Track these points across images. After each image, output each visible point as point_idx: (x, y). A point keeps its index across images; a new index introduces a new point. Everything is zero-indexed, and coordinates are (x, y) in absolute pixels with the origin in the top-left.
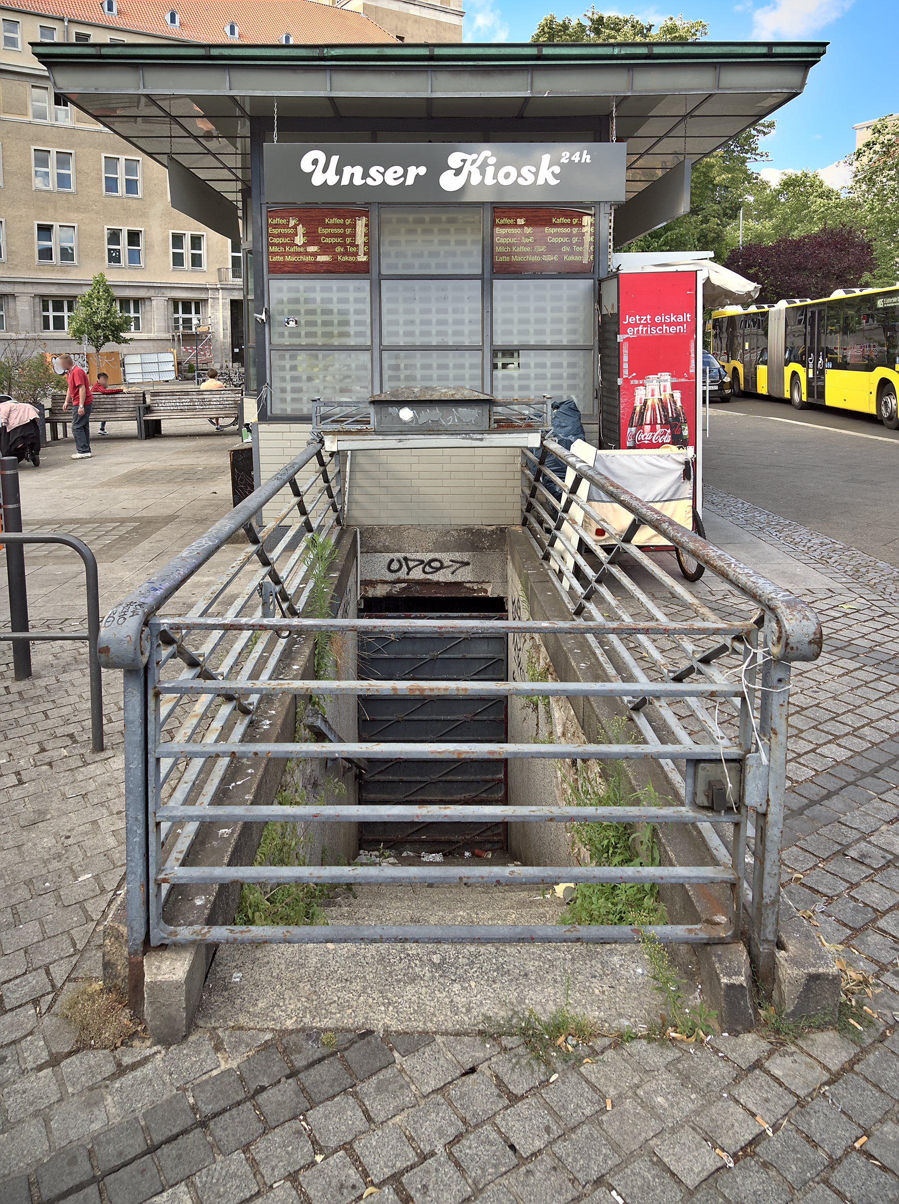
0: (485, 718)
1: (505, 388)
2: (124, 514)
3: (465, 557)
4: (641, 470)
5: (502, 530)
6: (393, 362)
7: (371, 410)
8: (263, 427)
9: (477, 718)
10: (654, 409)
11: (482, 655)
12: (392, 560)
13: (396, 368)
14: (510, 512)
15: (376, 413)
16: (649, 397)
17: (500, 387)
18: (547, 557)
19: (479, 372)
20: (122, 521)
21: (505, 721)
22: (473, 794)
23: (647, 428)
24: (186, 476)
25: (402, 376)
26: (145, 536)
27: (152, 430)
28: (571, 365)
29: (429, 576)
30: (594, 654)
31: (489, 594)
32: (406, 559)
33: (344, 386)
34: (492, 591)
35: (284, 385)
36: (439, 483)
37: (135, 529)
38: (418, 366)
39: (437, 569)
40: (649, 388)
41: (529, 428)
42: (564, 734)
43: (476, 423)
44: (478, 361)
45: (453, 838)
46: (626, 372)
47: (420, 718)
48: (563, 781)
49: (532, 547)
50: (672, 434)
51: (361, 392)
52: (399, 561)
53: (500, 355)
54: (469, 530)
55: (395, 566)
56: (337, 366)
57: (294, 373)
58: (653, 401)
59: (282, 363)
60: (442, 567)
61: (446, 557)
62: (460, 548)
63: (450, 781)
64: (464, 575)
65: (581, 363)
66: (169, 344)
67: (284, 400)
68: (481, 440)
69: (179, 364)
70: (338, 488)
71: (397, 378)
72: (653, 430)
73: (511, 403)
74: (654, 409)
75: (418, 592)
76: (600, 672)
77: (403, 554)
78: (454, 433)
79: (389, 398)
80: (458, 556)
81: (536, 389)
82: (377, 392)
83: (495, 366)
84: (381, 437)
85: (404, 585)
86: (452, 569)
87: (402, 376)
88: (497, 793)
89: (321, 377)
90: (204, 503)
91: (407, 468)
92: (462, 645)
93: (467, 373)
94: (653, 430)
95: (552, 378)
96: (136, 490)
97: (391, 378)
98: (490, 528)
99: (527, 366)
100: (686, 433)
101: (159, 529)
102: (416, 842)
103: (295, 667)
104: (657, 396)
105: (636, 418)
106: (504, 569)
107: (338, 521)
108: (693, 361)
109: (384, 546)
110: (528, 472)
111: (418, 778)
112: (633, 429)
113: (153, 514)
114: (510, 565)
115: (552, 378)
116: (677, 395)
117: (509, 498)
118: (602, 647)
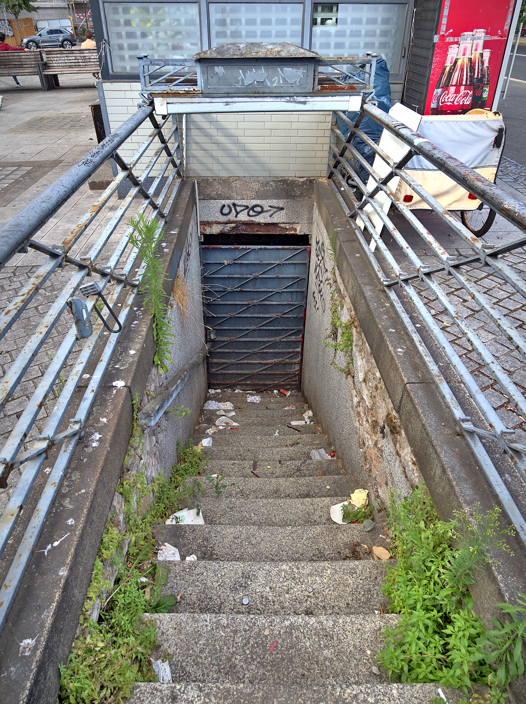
0: (290, 316)
1: (322, 46)
2: (22, 158)
3: (280, 203)
4: (456, 138)
5: (311, 181)
6: (219, 16)
7: (198, 69)
8: (107, 86)
9: (285, 316)
10: (462, 70)
11: (290, 276)
12: (224, 206)
13: (222, 23)
14: (320, 167)
15: (203, 73)
16: (460, 56)
17: (318, 45)
18: (354, 217)
19: (299, 28)
20: (20, 165)
21: (304, 318)
22: (280, 360)
23: (452, 89)
24: (73, 123)
25: (229, 32)
26: (35, 180)
27: (52, 84)
28: (385, 21)
29: (253, 219)
30: (412, 341)
31: (298, 232)
32: (234, 205)
33: (176, 42)
34: (300, 230)
35: (120, 41)
36: (261, 140)
37: (29, 172)
38: (243, 21)
39: (259, 213)
40: (462, 46)
41: (352, 90)
42: (364, 380)
43: (301, 84)
44: (299, 16)
45: (266, 383)
46: (443, 28)
47: (246, 315)
48: (358, 405)
49: (338, 201)
50: (473, 96)
51: (191, 49)
52: (229, 206)
53: (320, 9)
54: (284, 181)
55: (226, 210)
56: (168, 21)
57: (128, 29)
58: (463, 61)
59: (116, 17)
60: (262, 211)
61: (266, 203)
62: (276, 196)
63: (265, 353)
64: (279, 218)
65: (395, 19)
66: (66, 11)
67: (122, 58)
68: (304, 103)
69: (76, 28)
70: (176, 145)
71: (223, 34)
72: (457, 91)
73: (336, 62)
74: (462, 70)
75: (243, 230)
76: (417, 360)
77: (232, 201)
78: (278, 95)
79: (214, 55)
80: (275, 202)
81: (351, 47)
82: (206, 48)
83: (314, 22)
84: (208, 100)
85: (233, 225)
86: (270, 213)
87: (229, 32)
88: (296, 358)
89: (154, 32)
90: (82, 148)
91: (234, 125)
92: (276, 269)
93: (289, 28)
94: (457, 91)
95: (366, 36)
96: (34, 135)
97: (219, 34)
98: (301, 180)
99: (345, 22)
100: (485, 95)
101: (45, 173)
102: (243, 385)
103: (132, 352)
104: (468, 56)
105: (444, 78)
106: (311, 212)
107: (178, 173)
108: (510, 16)
109: (217, 194)
110: (338, 131)
111: (245, 351)
112: (440, 90)
113: (43, 159)
114: (316, 212)
115: (366, 36)
116: (487, 54)
117: (319, 154)
118: (414, 324)
